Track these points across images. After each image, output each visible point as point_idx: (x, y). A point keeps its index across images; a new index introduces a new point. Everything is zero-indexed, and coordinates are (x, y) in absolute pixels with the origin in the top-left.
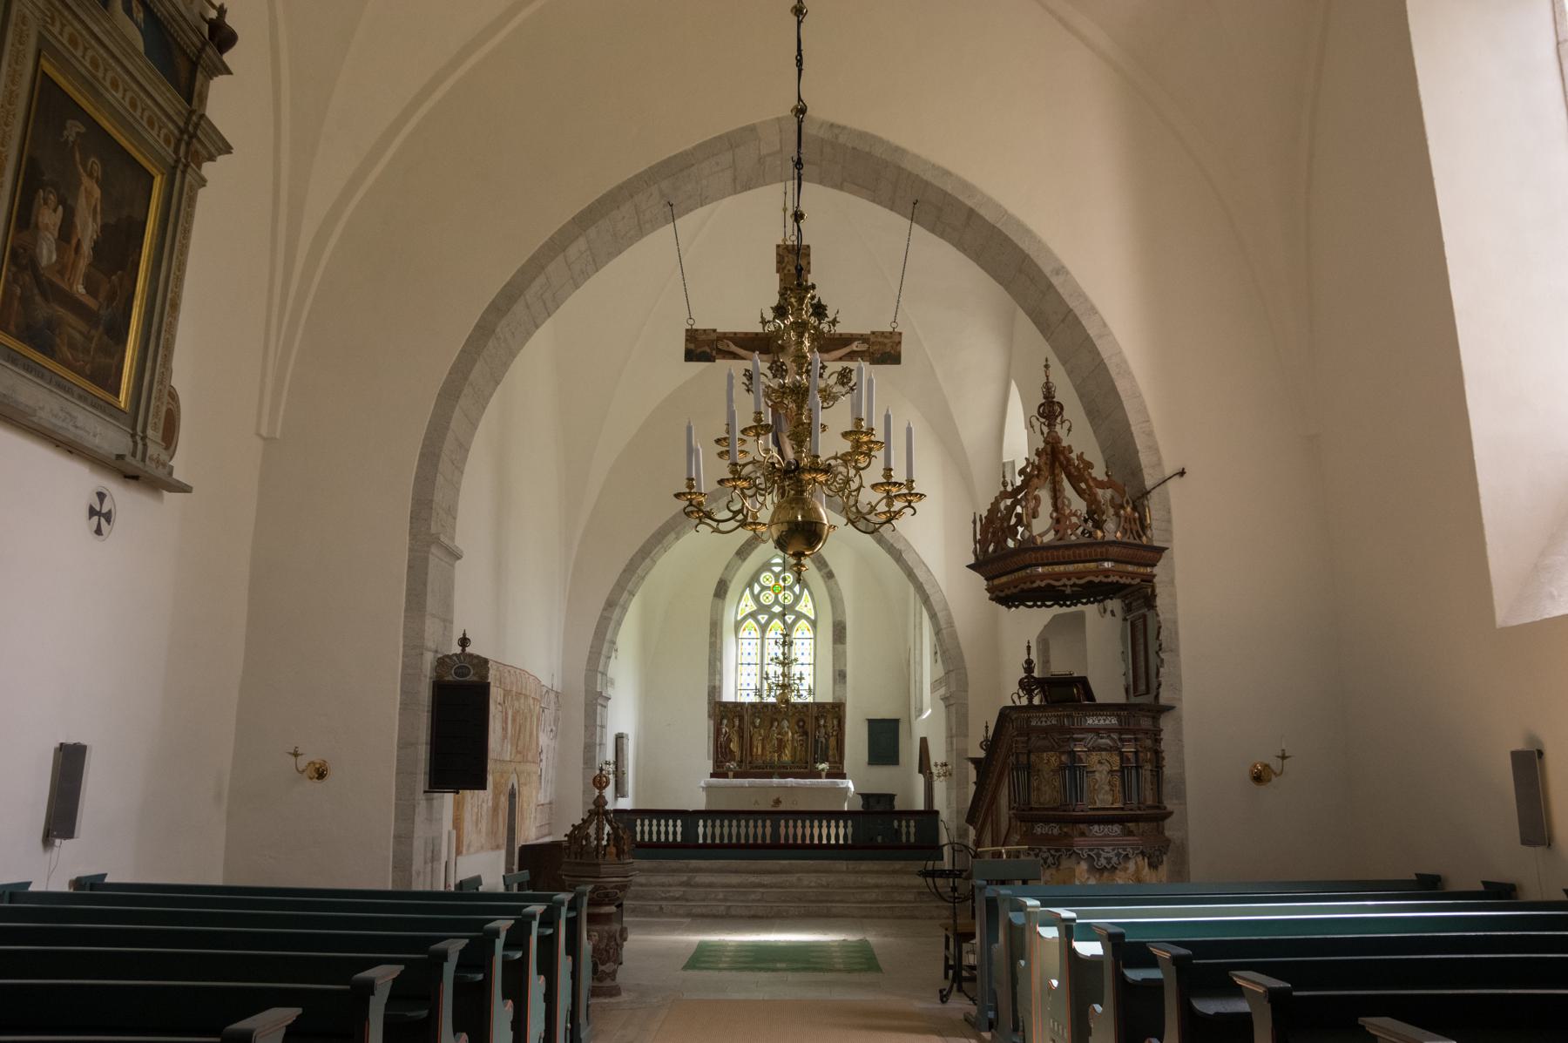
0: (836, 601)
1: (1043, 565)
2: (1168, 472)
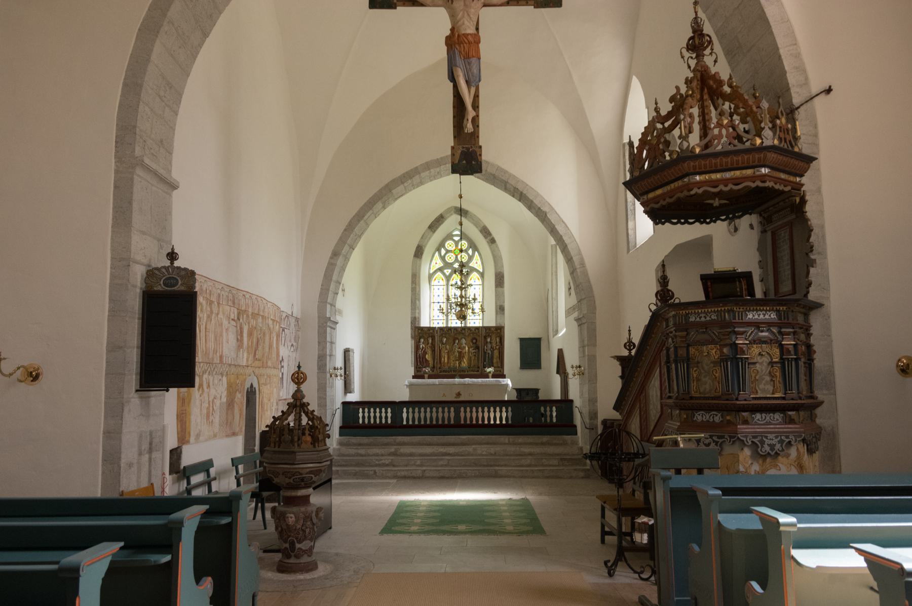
0: (497, 259)
1: (700, 173)
2: (815, 90)
